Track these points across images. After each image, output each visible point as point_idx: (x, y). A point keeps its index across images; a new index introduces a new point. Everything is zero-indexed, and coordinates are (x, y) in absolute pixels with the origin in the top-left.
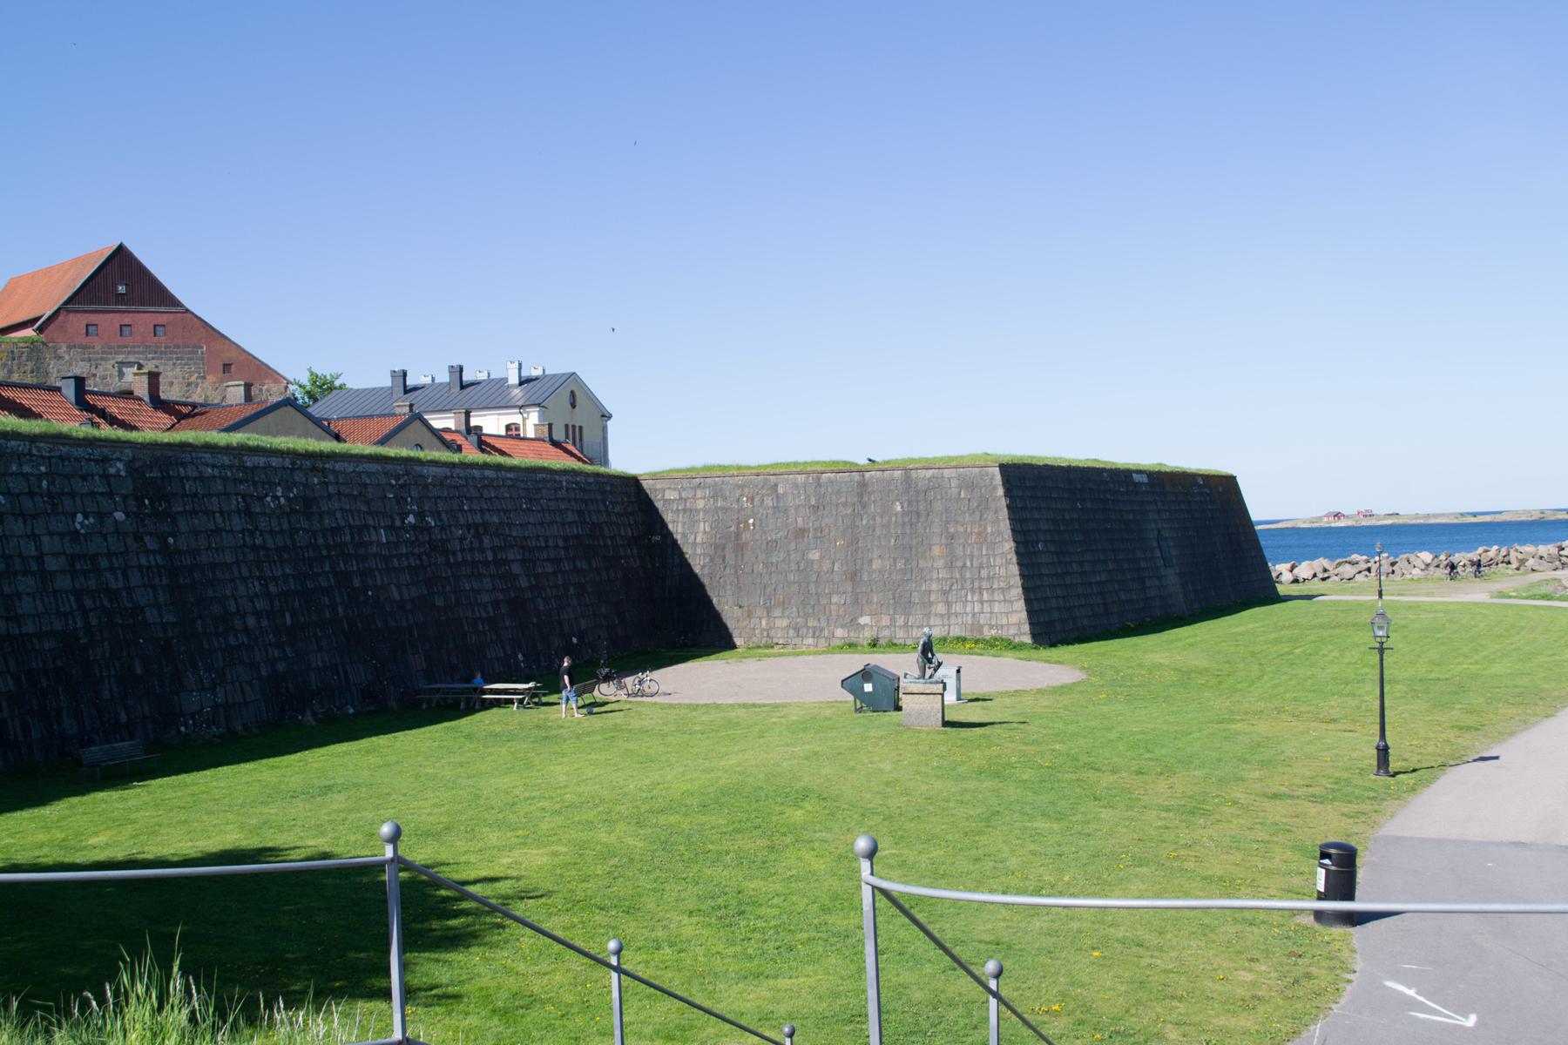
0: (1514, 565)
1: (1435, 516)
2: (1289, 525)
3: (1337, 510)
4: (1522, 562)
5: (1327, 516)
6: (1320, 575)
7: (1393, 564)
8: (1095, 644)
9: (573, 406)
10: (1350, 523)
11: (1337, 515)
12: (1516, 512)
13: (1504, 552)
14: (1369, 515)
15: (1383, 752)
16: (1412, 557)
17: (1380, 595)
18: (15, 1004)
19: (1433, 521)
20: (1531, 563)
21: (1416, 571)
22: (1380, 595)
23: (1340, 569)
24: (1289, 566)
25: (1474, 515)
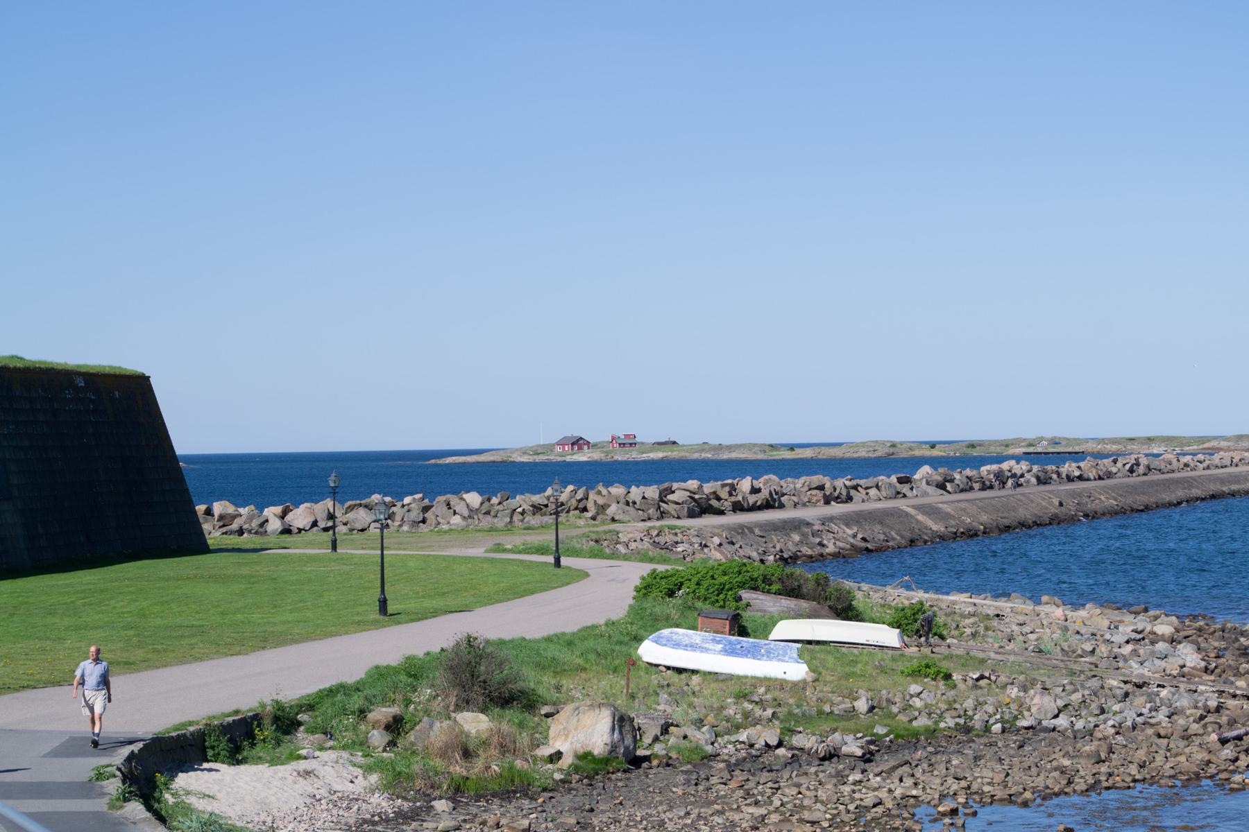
0: (589, 514)
1: (730, 448)
2: (497, 458)
3: (577, 433)
4: (602, 508)
5: (562, 443)
6: (322, 524)
7: (426, 509)
8: (80, 573)
9: (674, 443)
10: (596, 456)
11: (578, 443)
12: (851, 445)
13: (580, 495)
14: (629, 443)
15: (383, 604)
16: (454, 500)
17: (334, 548)
18: (478, 552)
19: (725, 456)
20: (613, 509)
21: (456, 520)
22: (334, 548)
23: (351, 516)
24: (278, 509)
25: (792, 448)
